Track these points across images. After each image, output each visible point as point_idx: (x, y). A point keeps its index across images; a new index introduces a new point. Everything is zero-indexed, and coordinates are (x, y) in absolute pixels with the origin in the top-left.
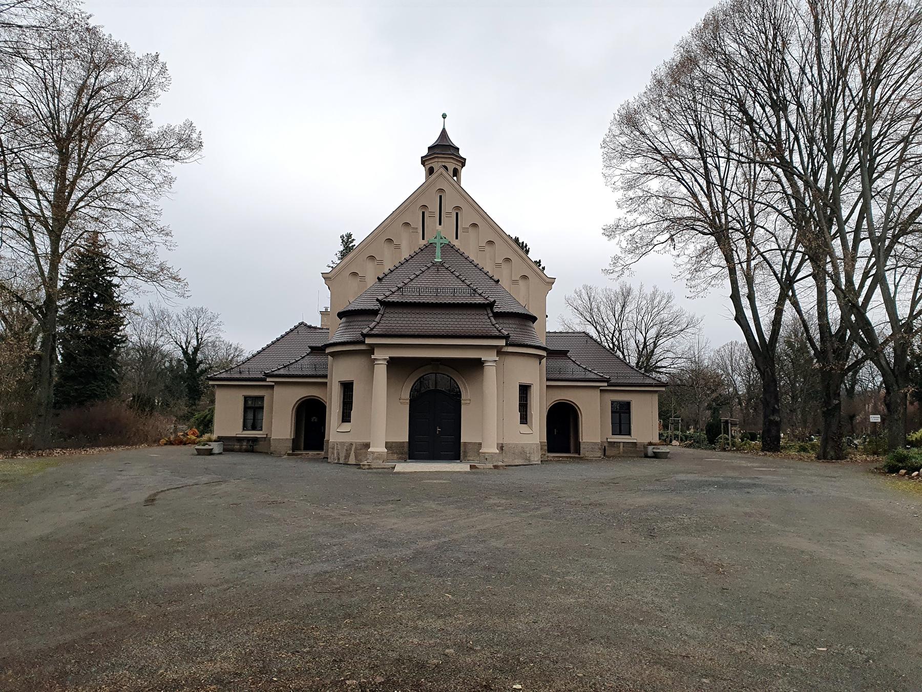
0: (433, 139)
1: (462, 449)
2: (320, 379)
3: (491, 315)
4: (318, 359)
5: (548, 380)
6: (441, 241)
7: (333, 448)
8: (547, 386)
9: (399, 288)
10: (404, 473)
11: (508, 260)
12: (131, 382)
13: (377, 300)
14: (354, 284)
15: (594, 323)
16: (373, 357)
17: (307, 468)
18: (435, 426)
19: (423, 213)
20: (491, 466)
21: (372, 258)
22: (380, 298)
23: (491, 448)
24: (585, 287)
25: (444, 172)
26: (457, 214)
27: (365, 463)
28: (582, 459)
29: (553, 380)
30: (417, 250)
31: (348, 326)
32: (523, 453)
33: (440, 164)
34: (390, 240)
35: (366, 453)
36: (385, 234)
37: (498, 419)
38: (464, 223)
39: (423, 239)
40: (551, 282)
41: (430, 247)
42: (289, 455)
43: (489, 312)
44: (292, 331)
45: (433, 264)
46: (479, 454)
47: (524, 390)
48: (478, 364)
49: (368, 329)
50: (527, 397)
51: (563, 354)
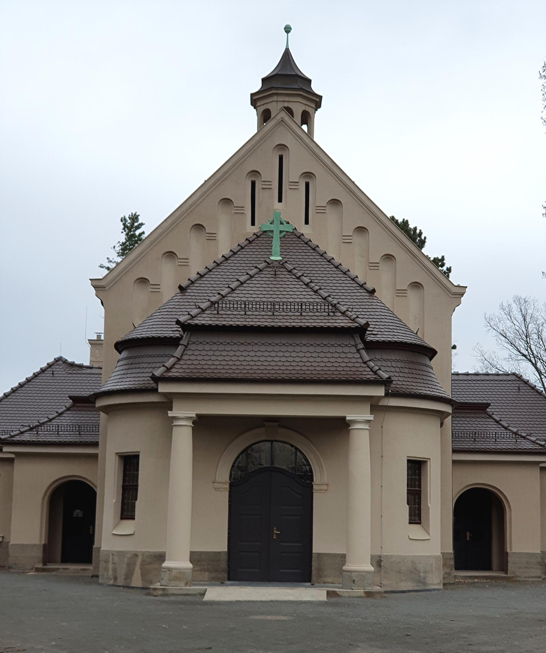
0: (269, 66)
1: (314, 564)
2: (87, 447)
3: (361, 346)
4: (83, 417)
5: (455, 451)
6: (282, 228)
7: (107, 562)
8: (454, 462)
9: (213, 303)
10: (219, 603)
11: (389, 257)
12: (364, 327)
13: (178, 322)
14: (141, 296)
15: (531, 358)
16: (170, 414)
17: (65, 590)
18: (271, 526)
19: (253, 184)
20: (360, 592)
21: (171, 254)
22: (182, 319)
23: (360, 563)
24: (517, 300)
25: (287, 118)
26: (307, 185)
27: (158, 585)
28: (512, 581)
29: (463, 450)
30: (243, 242)
31: (131, 364)
32: (414, 571)
33: (281, 105)
34: (199, 227)
35: (159, 570)
36: (191, 217)
37: (373, 513)
38: (319, 198)
39: (253, 224)
40: (458, 293)
41: (264, 237)
42: (37, 570)
43: (359, 341)
44: (43, 371)
45: (269, 264)
46: (342, 571)
47: (416, 467)
48: (341, 426)
49: (163, 369)
50: (420, 480)
51: (480, 409)
